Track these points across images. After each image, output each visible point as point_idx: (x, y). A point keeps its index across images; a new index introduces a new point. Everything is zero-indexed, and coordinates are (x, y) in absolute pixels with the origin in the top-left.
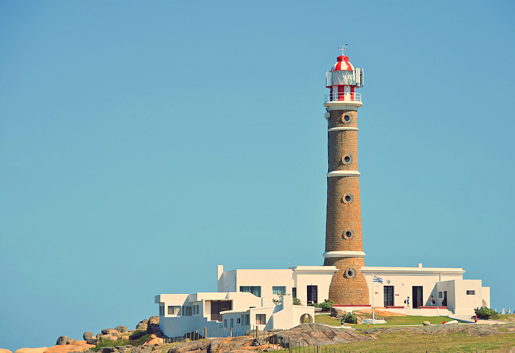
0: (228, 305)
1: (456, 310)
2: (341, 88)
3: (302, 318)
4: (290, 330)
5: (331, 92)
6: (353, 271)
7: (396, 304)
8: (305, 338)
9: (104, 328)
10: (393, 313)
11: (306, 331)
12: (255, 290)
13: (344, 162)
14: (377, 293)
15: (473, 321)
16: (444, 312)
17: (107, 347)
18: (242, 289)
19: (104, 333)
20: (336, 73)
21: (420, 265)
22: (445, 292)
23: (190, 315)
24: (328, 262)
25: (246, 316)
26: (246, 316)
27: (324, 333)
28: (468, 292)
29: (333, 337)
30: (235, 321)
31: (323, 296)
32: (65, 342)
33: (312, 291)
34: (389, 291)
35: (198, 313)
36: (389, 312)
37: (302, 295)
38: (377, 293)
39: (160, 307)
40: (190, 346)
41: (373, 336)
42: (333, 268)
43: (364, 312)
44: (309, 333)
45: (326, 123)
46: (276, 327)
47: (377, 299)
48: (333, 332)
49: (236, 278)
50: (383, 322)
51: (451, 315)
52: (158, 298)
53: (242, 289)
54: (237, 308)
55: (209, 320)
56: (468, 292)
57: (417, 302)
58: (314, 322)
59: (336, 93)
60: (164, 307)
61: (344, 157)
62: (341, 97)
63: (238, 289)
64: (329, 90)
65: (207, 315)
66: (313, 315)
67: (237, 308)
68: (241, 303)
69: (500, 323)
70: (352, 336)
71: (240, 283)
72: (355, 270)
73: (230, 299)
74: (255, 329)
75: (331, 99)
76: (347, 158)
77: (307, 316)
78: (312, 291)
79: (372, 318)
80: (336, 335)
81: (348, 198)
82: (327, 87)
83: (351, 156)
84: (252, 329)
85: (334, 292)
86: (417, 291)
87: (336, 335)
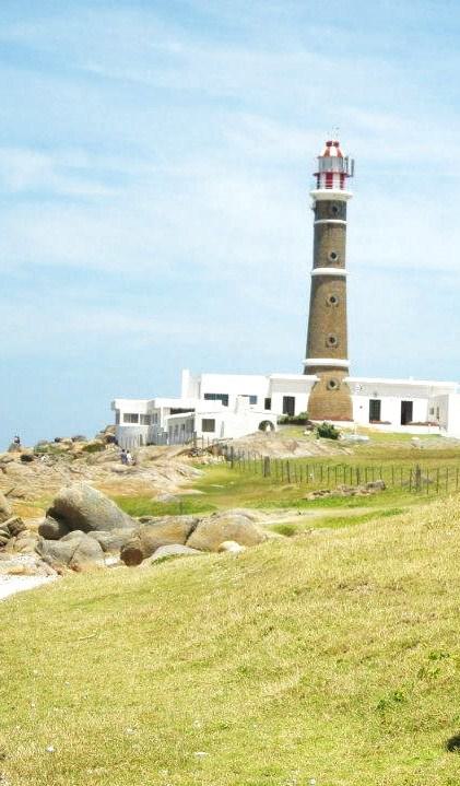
2: (330, 176)
6: (335, 382)
7: (383, 418)
9: (59, 436)
16: (434, 430)
17: (330, 423)
18: (208, 397)
19: (57, 441)
20: (327, 159)
21: (411, 378)
24: (309, 370)
27: (283, 443)
29: (294, 449)
30: (180, 428)
41: (347, 449)
42: (313, 378)
45: (313, 215)
47: (361, 414)
49: (310, 335)
52: (113, 404)
53: (208, 397)
59: (323, 180)
61: (329, 253)
62: (329, 185)
75: (318, 187)
76: (334, 256)
80: (298, 446)
81: (333, 300)
85: (313, 405)
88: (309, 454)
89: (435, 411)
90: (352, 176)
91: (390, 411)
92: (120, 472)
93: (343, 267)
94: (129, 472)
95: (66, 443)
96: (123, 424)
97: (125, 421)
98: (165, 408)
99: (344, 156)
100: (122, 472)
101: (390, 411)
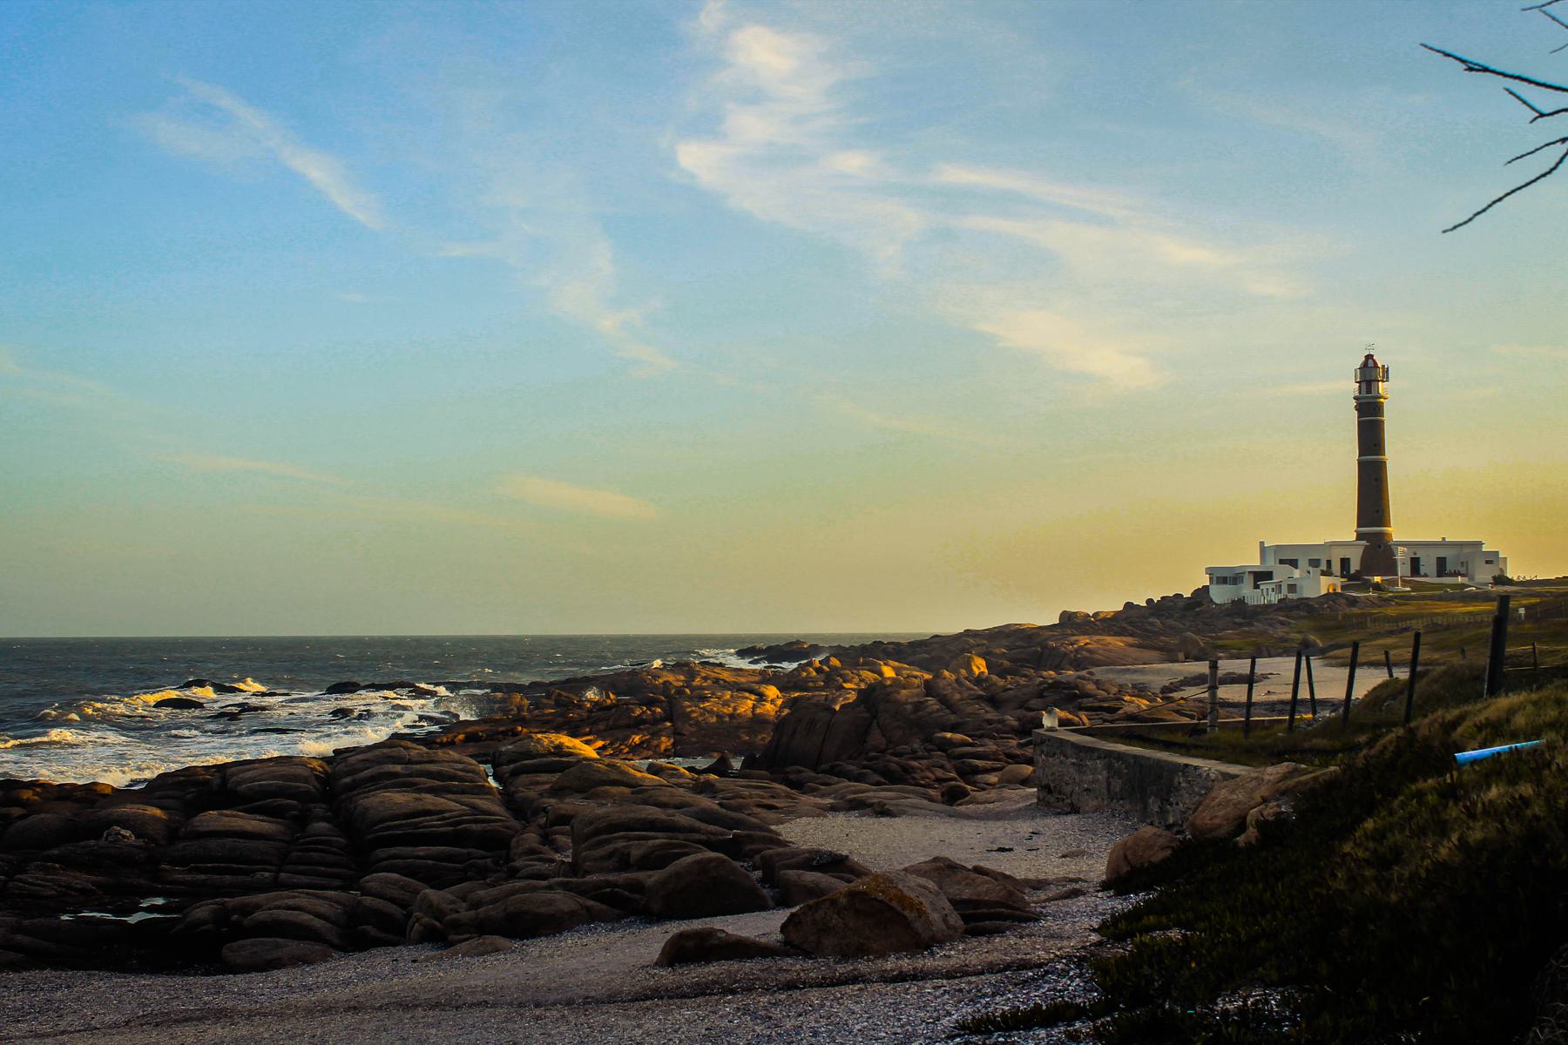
31: (1355, 566)
33: (1345, 563)
37: (1336, 567)
46: (1306, 595)
47: (1403, 569)
78: (1345, 563)
86: (1441, 562)
91: (1428, 565)
92: (1241, 625)
101: (1428, 565)
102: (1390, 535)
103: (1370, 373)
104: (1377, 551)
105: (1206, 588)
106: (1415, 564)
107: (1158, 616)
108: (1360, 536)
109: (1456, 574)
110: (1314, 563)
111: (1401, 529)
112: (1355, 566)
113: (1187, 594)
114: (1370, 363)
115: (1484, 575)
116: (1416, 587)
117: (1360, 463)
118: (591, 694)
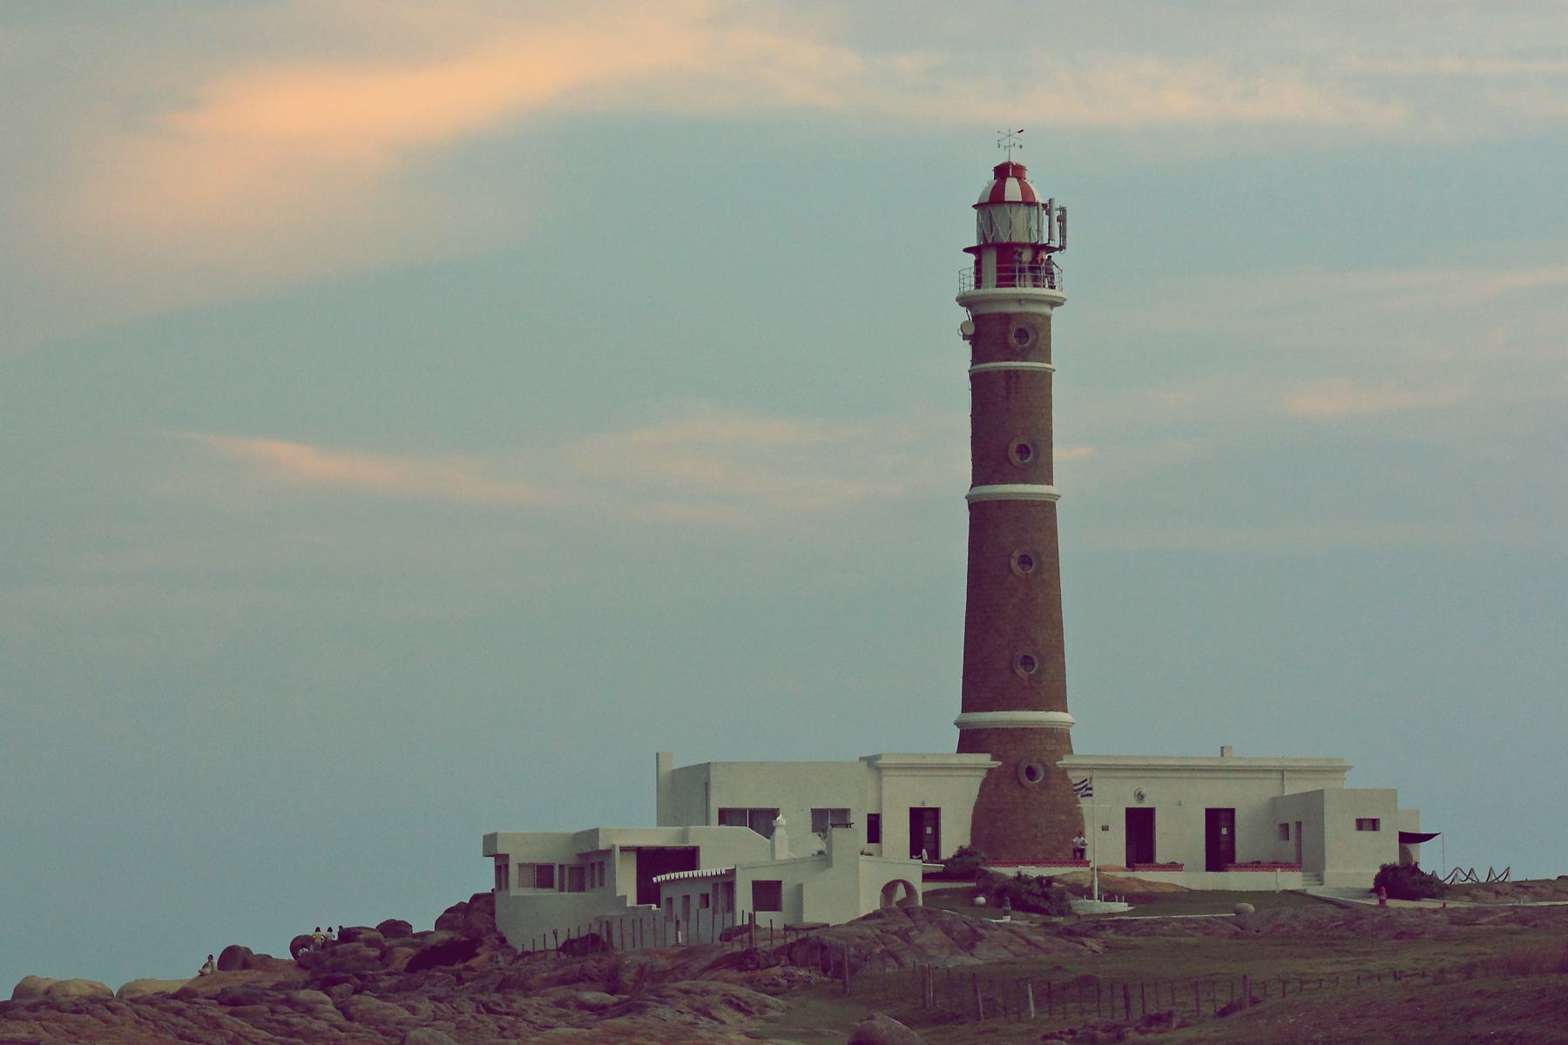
0: (687, 857)
1: (1329, 872)
3: (889, 889)
4: (851, 924)
5: (978, 263)
7: (1161, 857)
8: (890, 947)
10: (1150, 884)
11: (896, 928)
12: (762, 820)
13: (1015, 458)
14: (1105, 828)
15: (1375, 902)
16: (1292, 880)
18: (726, 816)
20: (997, 212)
22: (1299, 824)
23: (581, 888)
25: (726, 883)
26: (726, 883)
27: (948, 932)
28: (1360, 824)
29: (973, 945)
30: (695, 901)
31: (954, 836)
32: (1176, 1021)
33: (924, 823)
34: (1140, 824)
35: (601, 884)
36: (1140, 881)
37: (897, 831)
38: (1105, 828)
39: (498, 868)
40: (560, 972)
41: (1089, 942)
42: (984, 759)
43: (1070, 880)
44: (905, 935)
45: (966, 349)
46: (810, 917)
47: (1106, 847)
48: (973, 931)
50: (1122, 907)
51: (1314, 890)
53: (726, 816)
54: (708, 867)
55: (632, 900)
56: (1360, 824)
57: (1219, 854)
58: (920, 903)
60: (507, 866)
63: (715, 816)
64: (972, 257)
65: (626, 881)
66: (920, 887)
67: (708, 867)
68: (721, 850)
69: (1450, 905)
70: (1029, 942)
71: (719, 801)
72: (1043, 764)
73: (692, 843)
74: (746, 922)
76: (1023, 450)
77: (901, 888)
78: (924, 823)
79: (1091, 897)
80: (981, 938)
82: (967, 250)
83: (1034, 445)
84: (739, 923)
86: (1219, 821)
87: (981, 938)
88: (1005, 955)
89: (1292, 829)
90: (1061, 248)
91: (1180, 836)
92: (600, 1010)
93: (1050, 483)
94: (625, 1009)
95: (370, 943)
96: (515, 890)
97: (521, 885)
98: (624, 849)
99: (1040, 198)
100: (604, 1007)
101: (1180, 836)
102: (1060, 738)
103: (1011, 251)
104: (1024, 781)
105: (483, 903)
106: (1140, 824)
107: (326, 985)
108: (970, 740)
109: (1173, 866)
110: (827, 820)
111: (1120, 710)
112: (954, 836)
113: (423, 922)
114: (1012, 189)
115: (1351, 866)
116: (1144, 899)
117: (977, 379)
118: (1224, 831)
